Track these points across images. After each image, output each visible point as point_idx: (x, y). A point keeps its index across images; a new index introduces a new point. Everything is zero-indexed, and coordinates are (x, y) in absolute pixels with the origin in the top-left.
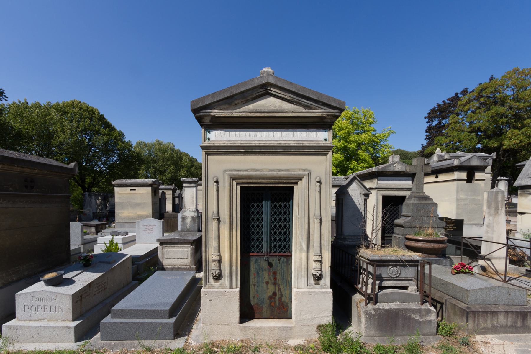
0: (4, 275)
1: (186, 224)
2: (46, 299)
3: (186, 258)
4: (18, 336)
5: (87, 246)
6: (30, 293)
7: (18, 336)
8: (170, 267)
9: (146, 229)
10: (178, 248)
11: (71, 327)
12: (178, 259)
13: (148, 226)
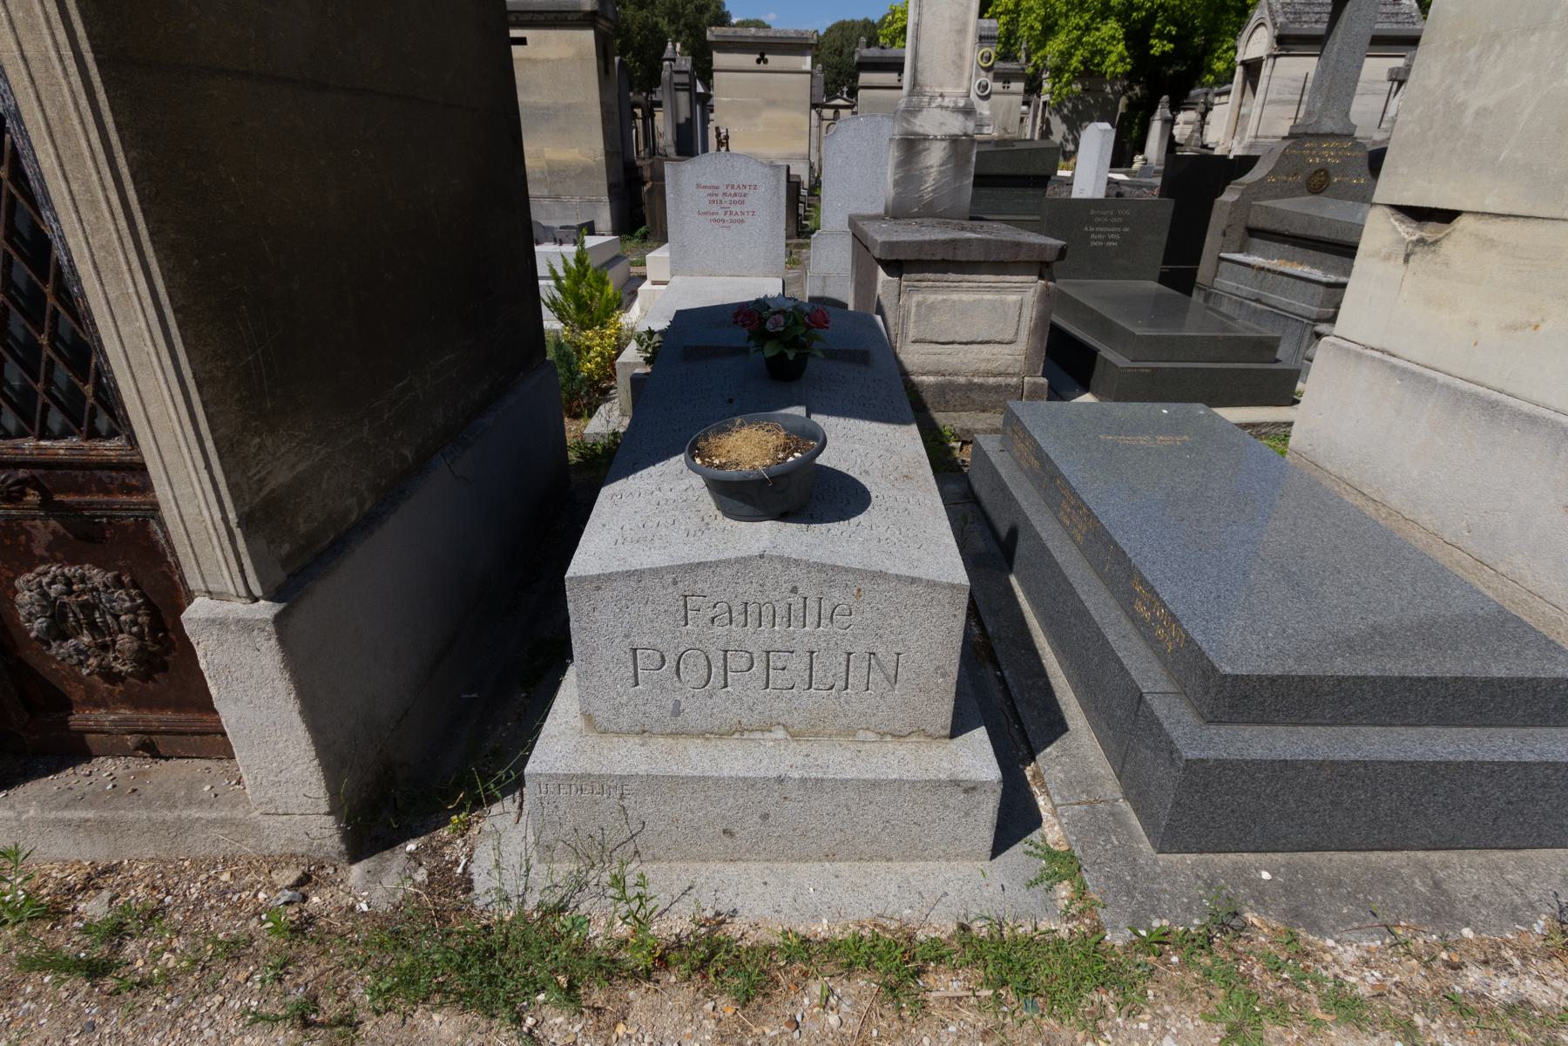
1: (920, 179)
2: (781, 610)
3: (1008, 338)
4: (636, 828)
6: (670, 569)
7: (636, 828)
8: (931, 379)
9: (715, 208)
10: (978, 290)
11: (983, 783)
12: (971, 343)
13: (722, 189)
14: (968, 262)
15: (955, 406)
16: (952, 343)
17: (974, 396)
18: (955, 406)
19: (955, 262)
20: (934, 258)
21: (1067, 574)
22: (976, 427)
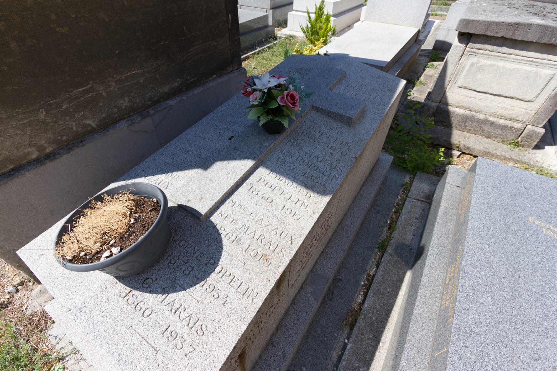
0: (42, 115)
5: (279, 11)
10: (521, 62)
12: (499, 96)
14: (522, 42)
15: (470, 130)
16: (485, 93)
17: (485, 127)
18: (470, 130)
19: (511, 40)
20: (496, 35)
21: (411, 330)
22: (475, 147)
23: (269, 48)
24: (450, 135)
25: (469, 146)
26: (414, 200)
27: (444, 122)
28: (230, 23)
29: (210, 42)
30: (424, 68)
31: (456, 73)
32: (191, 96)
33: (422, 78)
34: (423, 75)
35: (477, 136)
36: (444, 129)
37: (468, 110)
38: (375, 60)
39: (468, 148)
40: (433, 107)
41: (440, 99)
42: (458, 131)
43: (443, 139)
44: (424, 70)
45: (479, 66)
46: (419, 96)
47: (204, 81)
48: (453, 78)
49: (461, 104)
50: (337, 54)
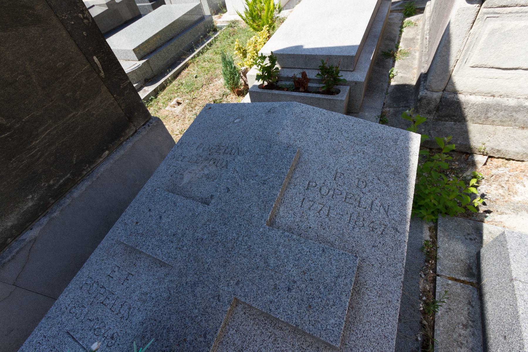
18: (494, 121)
23: (210, 45)
24: (465, 134)
25: (500, 149)
26: (450, 282)
27: (454, 116)
28: (101, 69)
29: (72, 115)
30: (400, 29)
31: (465, 48)
32: (69, 204)
33: (401, 45)
34: (402, 40)
35: (505, 128)
36: (455, 124)
37: (489, 95)
38: (339, 48)
39: (498, 151)
40: (435, 99)
41: (443, 87)
42: (476, 125)
43: (459, 142)
44: (401, 32)
45: (504, 32)
46: (405, 75)
47: (89, 169)
48: (462, 55)
49: (477, 90)
50: (287, 48)
